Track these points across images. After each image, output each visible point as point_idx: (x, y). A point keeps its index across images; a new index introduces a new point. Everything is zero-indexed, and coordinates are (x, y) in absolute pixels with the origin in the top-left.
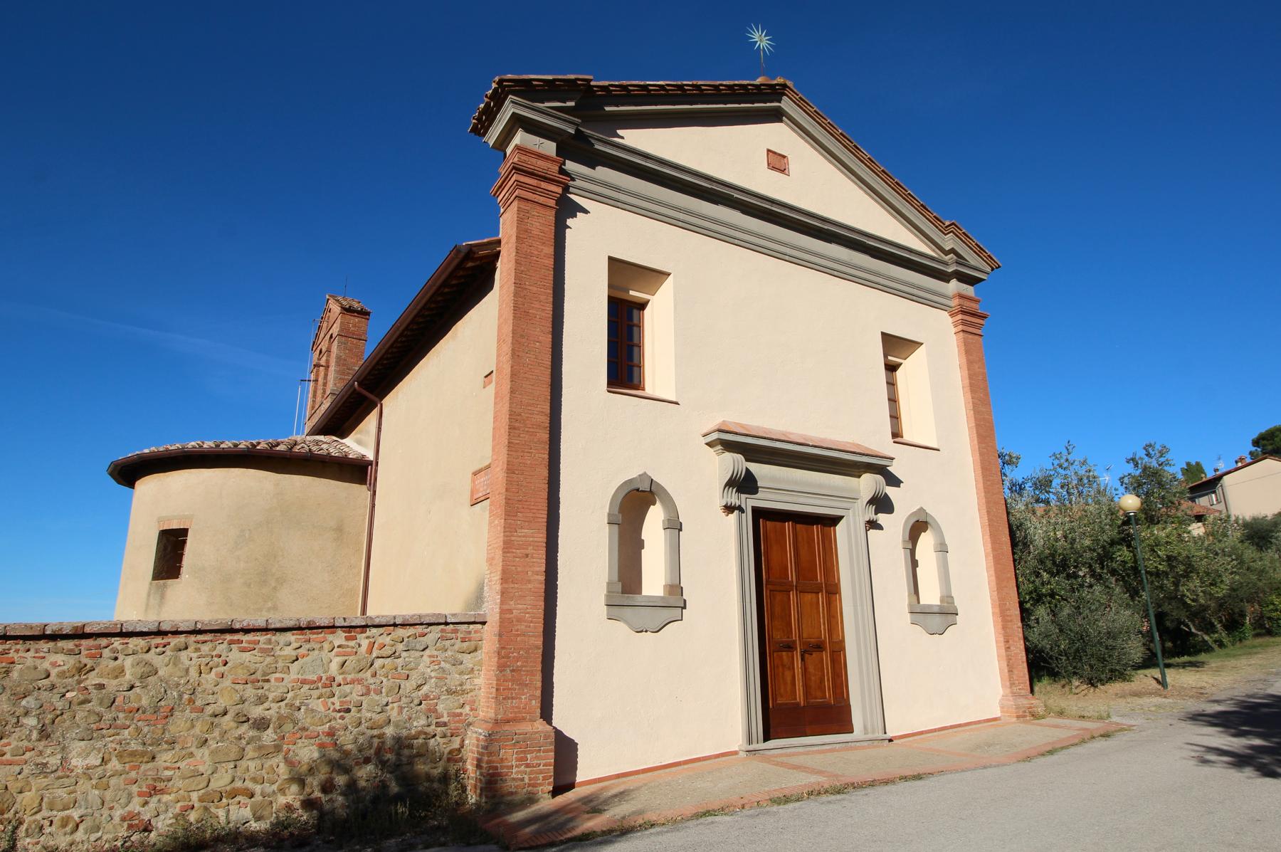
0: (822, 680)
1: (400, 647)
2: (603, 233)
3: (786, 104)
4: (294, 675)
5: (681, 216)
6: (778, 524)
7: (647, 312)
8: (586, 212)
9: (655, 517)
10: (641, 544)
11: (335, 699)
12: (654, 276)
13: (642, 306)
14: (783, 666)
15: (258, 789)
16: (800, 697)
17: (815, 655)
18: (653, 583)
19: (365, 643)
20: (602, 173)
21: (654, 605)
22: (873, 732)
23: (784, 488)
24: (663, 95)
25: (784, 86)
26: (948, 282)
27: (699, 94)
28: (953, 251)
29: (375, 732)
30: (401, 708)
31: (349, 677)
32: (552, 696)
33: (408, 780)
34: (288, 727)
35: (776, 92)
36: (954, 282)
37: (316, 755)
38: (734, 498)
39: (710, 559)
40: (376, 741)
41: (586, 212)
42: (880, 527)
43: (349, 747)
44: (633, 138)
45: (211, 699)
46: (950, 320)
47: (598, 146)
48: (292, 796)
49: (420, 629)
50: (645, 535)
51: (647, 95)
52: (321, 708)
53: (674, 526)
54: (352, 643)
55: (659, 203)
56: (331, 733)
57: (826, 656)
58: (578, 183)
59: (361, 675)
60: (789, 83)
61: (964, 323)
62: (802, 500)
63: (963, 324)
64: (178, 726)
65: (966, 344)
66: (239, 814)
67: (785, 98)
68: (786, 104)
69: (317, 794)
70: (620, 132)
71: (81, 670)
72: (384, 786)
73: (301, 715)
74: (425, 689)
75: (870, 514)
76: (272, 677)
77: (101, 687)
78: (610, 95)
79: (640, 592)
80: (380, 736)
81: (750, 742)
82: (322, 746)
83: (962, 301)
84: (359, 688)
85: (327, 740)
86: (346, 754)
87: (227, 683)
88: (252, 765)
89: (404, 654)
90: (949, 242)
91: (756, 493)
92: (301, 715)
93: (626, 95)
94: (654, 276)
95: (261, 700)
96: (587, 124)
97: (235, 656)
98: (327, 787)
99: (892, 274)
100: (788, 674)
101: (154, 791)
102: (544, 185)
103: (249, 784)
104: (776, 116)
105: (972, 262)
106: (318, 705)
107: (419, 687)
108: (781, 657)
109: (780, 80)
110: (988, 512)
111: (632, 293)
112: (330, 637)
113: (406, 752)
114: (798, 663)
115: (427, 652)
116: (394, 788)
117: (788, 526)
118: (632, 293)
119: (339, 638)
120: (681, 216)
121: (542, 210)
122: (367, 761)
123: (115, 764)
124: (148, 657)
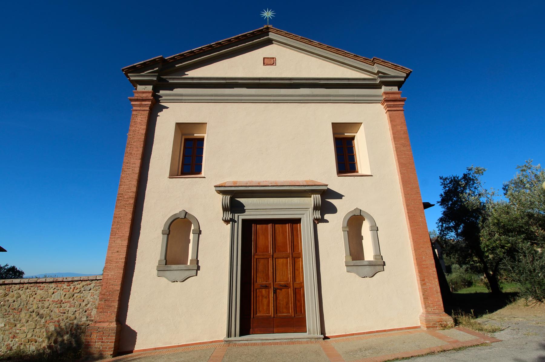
0: (287, 303)
1: (82, 289)
2: (175, 113)
3: (272, 36)
4: (51, 300)
5: (213, 98)
6: (264, 226)
7: (356, 142)
8: (167, 108)
9: (366, 228)
10: (362, 238)
11: (61, 309)
12: (355, 126)
13: (353, 138)
14: (262, 296)
15: (38, 339)
16: (272, 313)
17: (283, 290)
18: (369, 255)
19: (72, 287)
20: (177, 91)
21: (371, 264)
22: (314, 333)
23: (255, 208)
24: (202, 52)
25: (268, 28)
26: (381, 88)
27: (221, 46)
28: (379, 72)
29: (71, 322)
30: (80, 313)
31: (67, 300)
32: (127, 311)
33: (79, 342)
34: (48, 318)
35: (266, 32)
36: (383, 87)
37: (53, 329)
38: (229, 216)
39: (216, 246)
40: (71, 325)
41: (167, 108)
42: (327, 221)
43: (64, 327)
44: (191, 74)
45: (31, 306)
46: (383, 107)
47: (171, 81)
48: (45, 344)
49: (88, 282)
50: (363, 234)
51: (194, 55)
52: (57, 312)
53: (375, 229)
54: (69, 287)
55: (358, 96)
56: (58, 321)
57: (291, 291)
58: (164, 98)
59: (70, 300)
60: (269, 26)
61: (388, 106)
62: (252, 213)
63: (388, 107)
64: (23, 314)
65: (390, 117)
66: (32, 348)
67: (270, 33)
68: (272, 36)
69: (53, 344)
70: (186, 73)
71: (6, 295)
72: (70, 343)
73: (52, 314)
74: (89, 305)
75: (318, 215)
76: (46, 300)
77: (8, 300)
78: (175, 60)
79: (364, 259)
80: (72, 324)
81: (229, 335)
82: (55, 326)
83: (387, 96)
84: (68, 305)
85: (57, 324)
86: (62, 329)
87: (35, 301)
88: (38, 330)
89: (84, 292)
90: (376, 68)
91: (245, 212)
92: (52, 314)
93: (184, 58)
94: (355, 126)
95: (43, 307)
96: (166, 75)
97: (39, 292)
98: (56, 342)
99: (340, 93)
100: (265, 301)
101: (14, 337)
102: (143, 103)
103: (36, 338)
104: (269, 42)
105: (392, 74)
106: (56, 310)
107: (86, 305)
108: (262, 292)
109: (265, 26)
110: (407, 206)
111: (195, 135)
112: (63, 285)
113: (79, 331)
114: (272, 295)
115: (91, 291)
116: (74, 345)
117: (270, 226)
118: (195, 135)
119: (65, 286)
120: (213, 98)
121: (143, 112)
122: (67, 333)
123: (7, 327)
124: (19, 291)
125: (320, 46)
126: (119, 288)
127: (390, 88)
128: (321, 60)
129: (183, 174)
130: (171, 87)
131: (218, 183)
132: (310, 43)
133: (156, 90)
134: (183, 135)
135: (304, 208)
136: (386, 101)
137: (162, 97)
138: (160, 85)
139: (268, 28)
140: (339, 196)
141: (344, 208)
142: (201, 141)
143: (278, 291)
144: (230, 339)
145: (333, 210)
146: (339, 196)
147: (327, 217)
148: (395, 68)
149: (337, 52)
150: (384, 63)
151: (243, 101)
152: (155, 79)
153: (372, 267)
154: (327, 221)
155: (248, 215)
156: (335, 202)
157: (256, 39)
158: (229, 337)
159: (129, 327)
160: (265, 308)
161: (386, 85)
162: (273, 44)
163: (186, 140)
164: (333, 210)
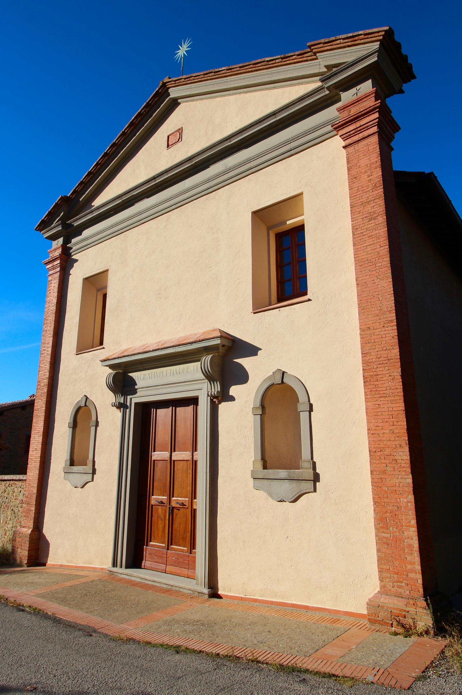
14: (158, 517)
20: (86, 233)
35: (163, 92)
42: (232, 399)
44: (97, 202)
47: (76, 224)
67: (170, 90)
68: (174, 93)
70: (93, 204)
78: (77, 193)
81: (114, 564)
104: (175, 104)
105: (350, 59)
111: (288, 222)
118: (288, 222)
125: (231, 73)
126: (35, 491)
127: (354, 90)
128: (242, 95)
129: (280, 300)
130: (78, 231)
131: (102, 358)
132: (218, 75)
133: (384, 90)
134: (269, 229)
135: (190, 378)
136: (338, 128)
137: (72, 248)
138: (70, 233)
139: (164, 84)
140: (252, 351)
141: (258, 370)
142: (300, 230)
143: (175, 510)
144: (115, 569)
145: (242, 377)
146: (252, 351)
147: (234, 390)
148: (353, 41)
149: (256, 68)
150: (331, 46)
151: (89, 246)
152: (60, 228)
153: (294, 484)
154: (232, 399)
155: (141, 396)
156: (245, 362)
157: (158, 107)
158: (114, 566)
159: (45, 536)
160: (160, 533)
161: (346, 89)
162: (179, 104)
163: (280, 237)
164: (242, 377)
